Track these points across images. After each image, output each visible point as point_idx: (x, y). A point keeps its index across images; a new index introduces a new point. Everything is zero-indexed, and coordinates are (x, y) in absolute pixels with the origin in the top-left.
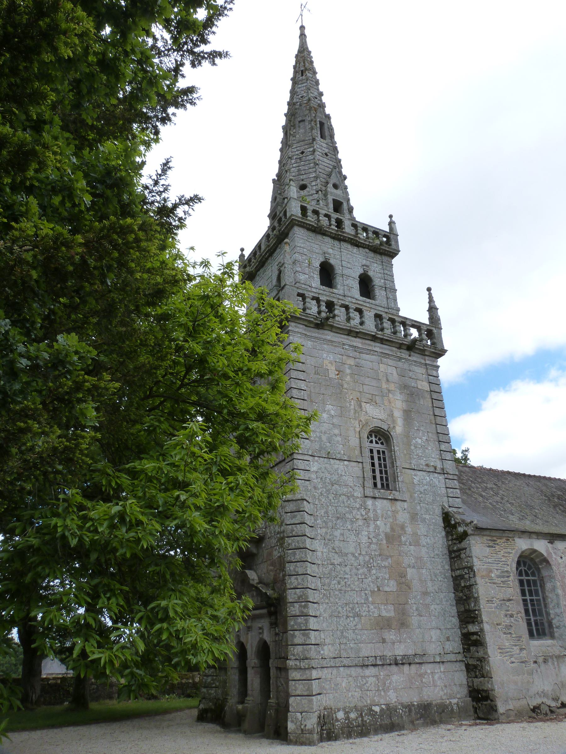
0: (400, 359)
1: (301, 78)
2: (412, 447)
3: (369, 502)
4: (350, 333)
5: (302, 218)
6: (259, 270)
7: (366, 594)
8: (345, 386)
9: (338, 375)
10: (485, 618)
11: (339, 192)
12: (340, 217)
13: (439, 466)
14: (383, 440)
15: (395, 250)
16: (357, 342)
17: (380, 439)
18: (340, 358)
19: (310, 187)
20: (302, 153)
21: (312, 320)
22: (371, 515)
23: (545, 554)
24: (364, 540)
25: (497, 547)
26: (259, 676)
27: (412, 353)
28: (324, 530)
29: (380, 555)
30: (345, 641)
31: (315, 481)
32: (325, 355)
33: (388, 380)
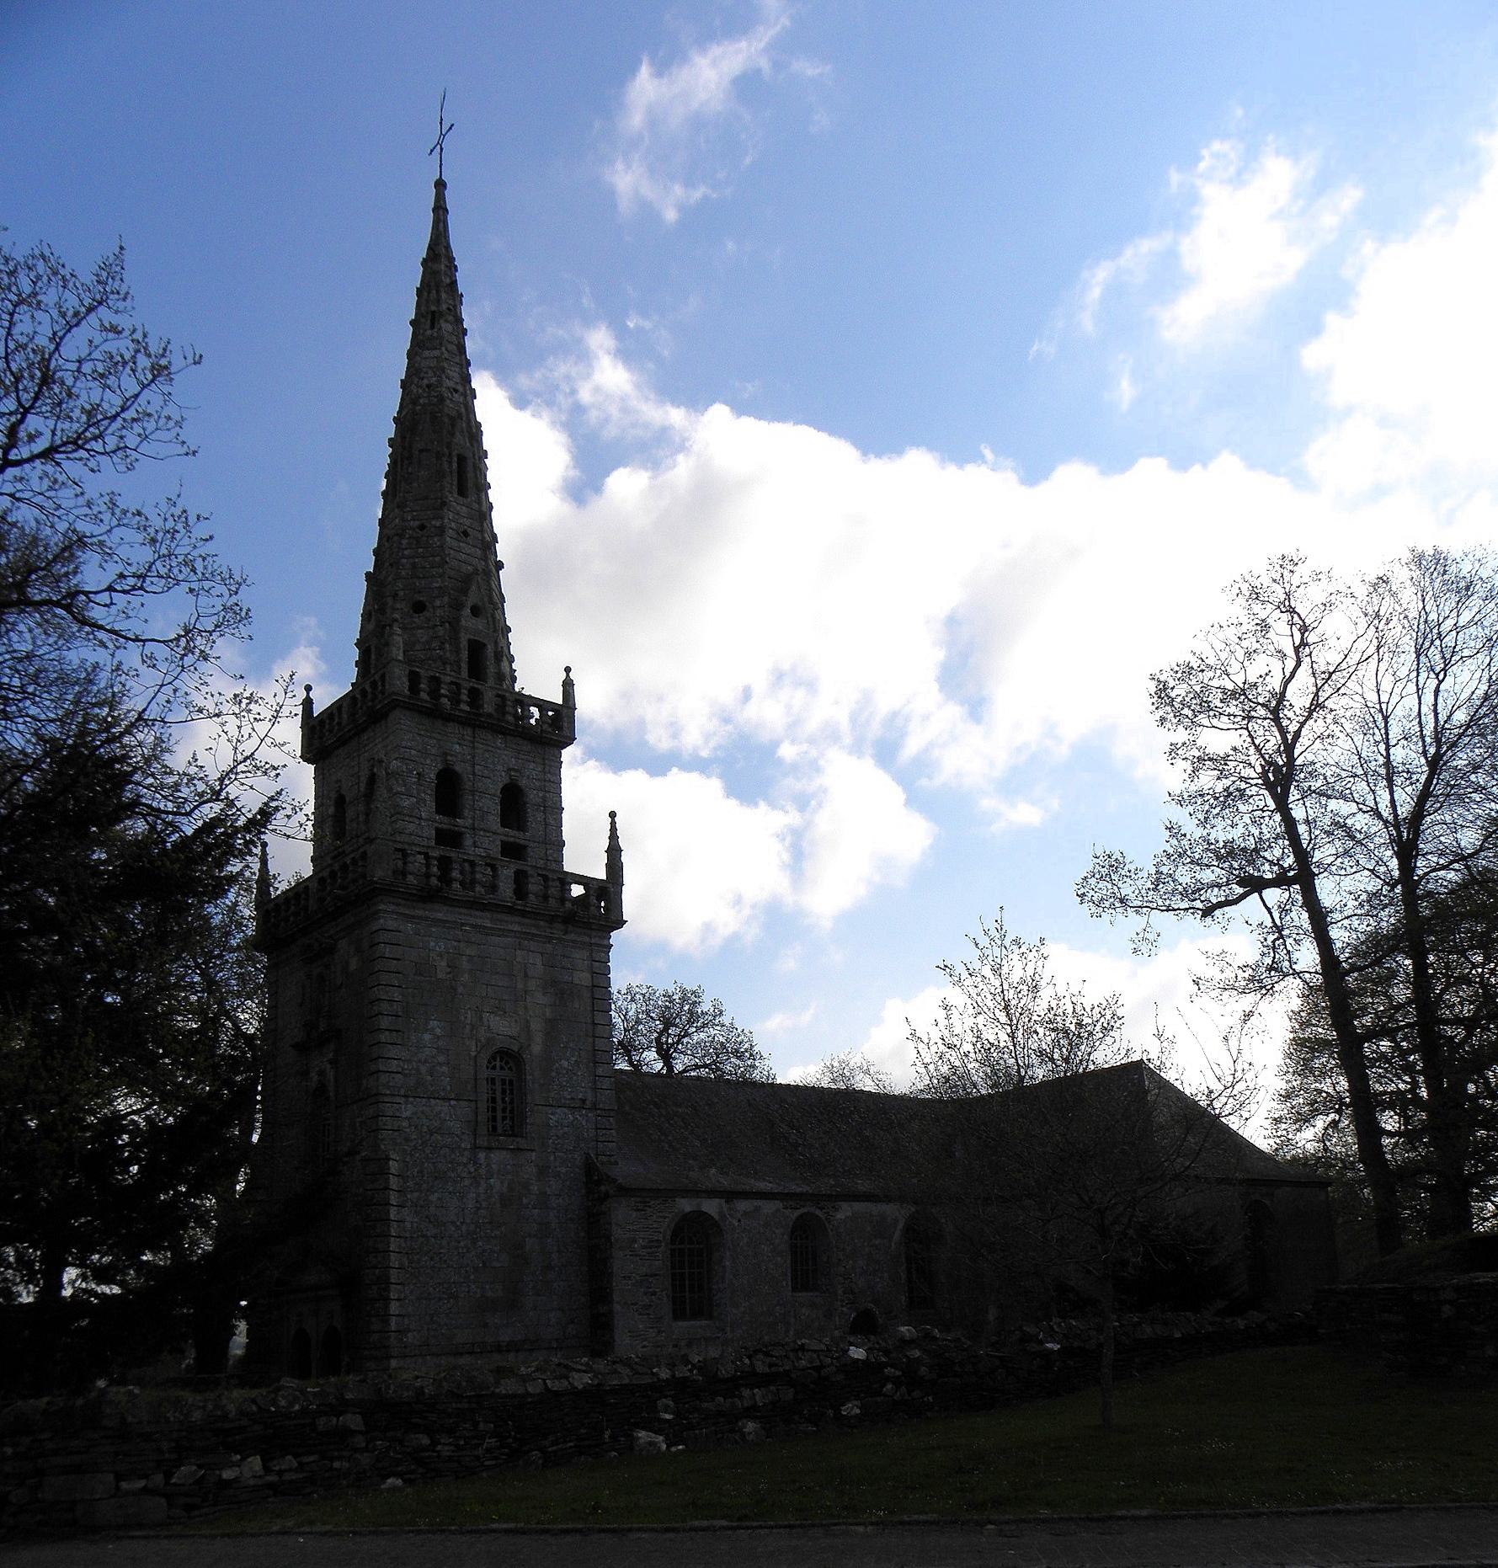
0: (549, 940)
1: (429, 332)
2: (554, 1074)
3: (482, 1155)
4: (475, 905)
5: (410, 698)
6: (338, 748)
7: (466, 1271)
8: (460, 989)
9: (450, 973)
10: (616, 1298)
11: (479, 624)
12: (476, 686)
13: (590, 1097)
14: (511, 1064)
15: (566, 737)
16: (485, 919)
17: (507, 1063)
18: (455, 948)
19: (431, 610)
20: (422, 527)
21: (414, 892)
22: (483, 1171)
23: (717, 1217)
24: (471, 1205)
25: (649, 1210)
26: (825, 1083)
27: (570, 928)
28: (416, 1194)
29: (490, 1223)
30: (435, 1326)
31: (408, 1130)
32: (432, 944)
33: (526, 975)
